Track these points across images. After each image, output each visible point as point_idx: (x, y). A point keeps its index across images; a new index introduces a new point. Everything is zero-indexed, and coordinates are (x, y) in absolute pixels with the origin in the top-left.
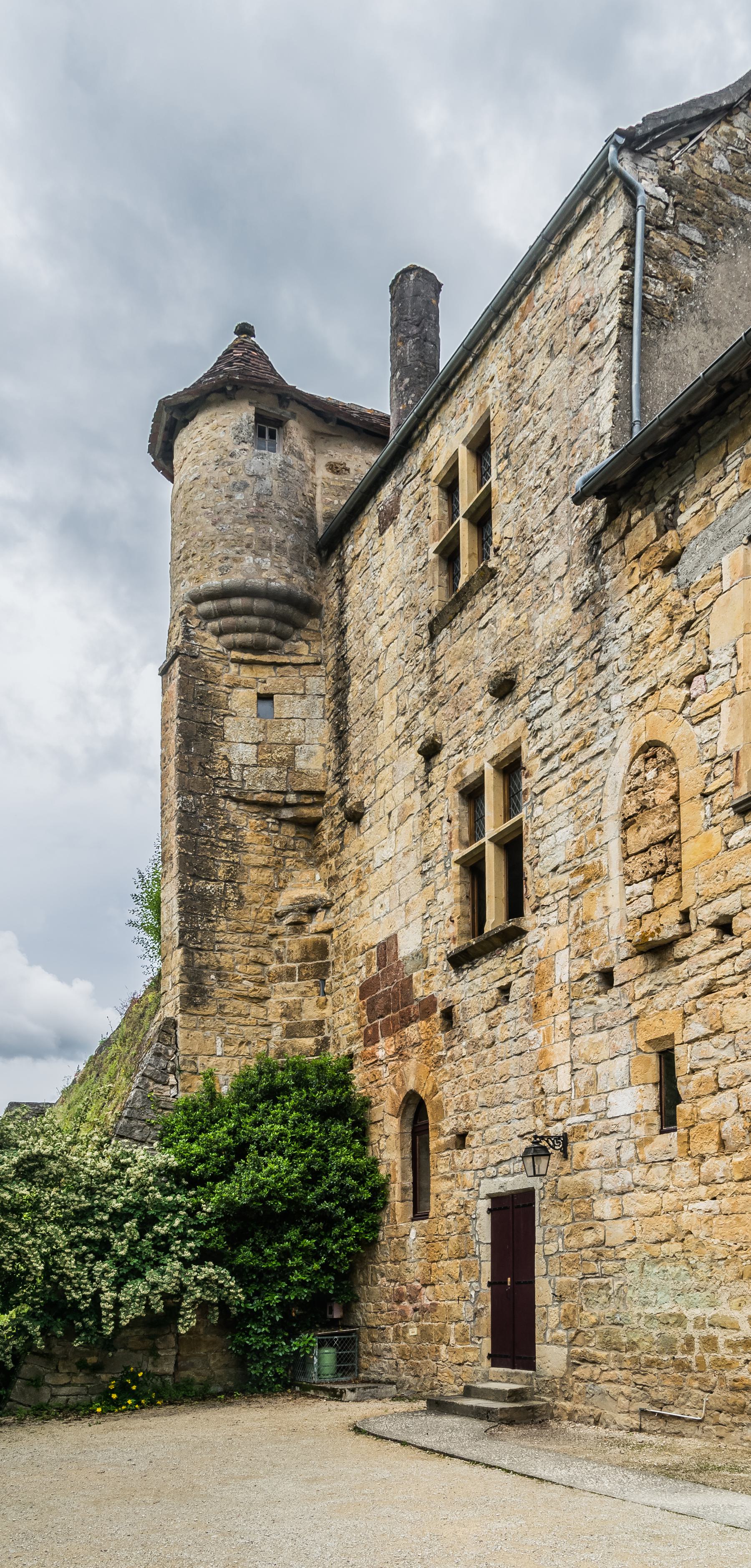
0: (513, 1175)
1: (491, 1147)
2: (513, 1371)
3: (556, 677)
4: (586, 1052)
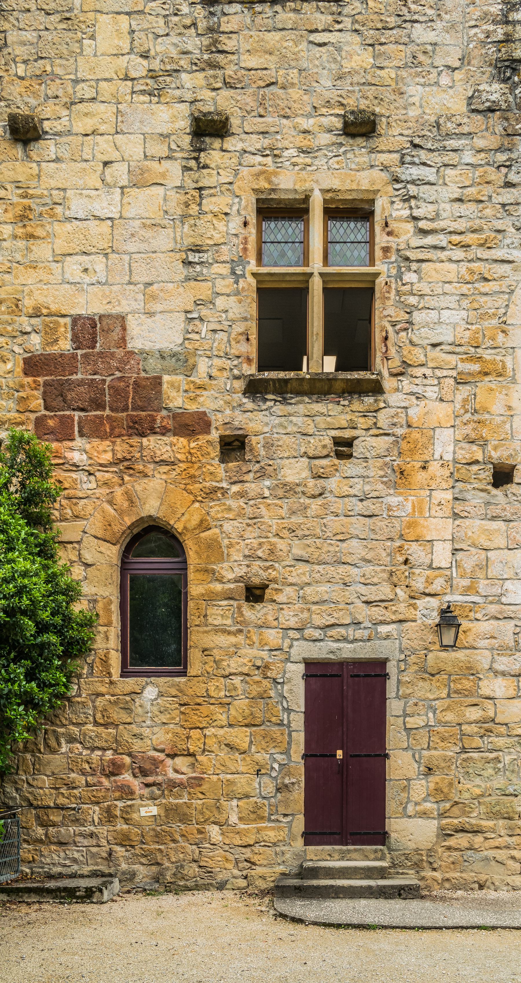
0: (352, 642)
1: (314, 608)
2: (344, 848)
3: (446, 160)
4: (475, 536)
